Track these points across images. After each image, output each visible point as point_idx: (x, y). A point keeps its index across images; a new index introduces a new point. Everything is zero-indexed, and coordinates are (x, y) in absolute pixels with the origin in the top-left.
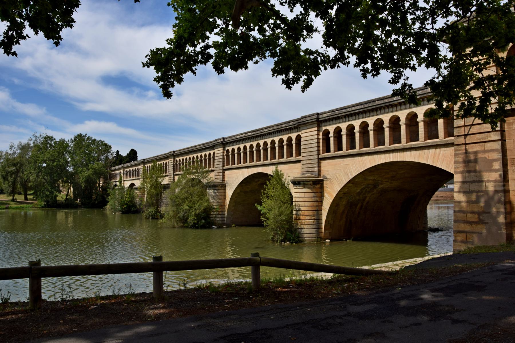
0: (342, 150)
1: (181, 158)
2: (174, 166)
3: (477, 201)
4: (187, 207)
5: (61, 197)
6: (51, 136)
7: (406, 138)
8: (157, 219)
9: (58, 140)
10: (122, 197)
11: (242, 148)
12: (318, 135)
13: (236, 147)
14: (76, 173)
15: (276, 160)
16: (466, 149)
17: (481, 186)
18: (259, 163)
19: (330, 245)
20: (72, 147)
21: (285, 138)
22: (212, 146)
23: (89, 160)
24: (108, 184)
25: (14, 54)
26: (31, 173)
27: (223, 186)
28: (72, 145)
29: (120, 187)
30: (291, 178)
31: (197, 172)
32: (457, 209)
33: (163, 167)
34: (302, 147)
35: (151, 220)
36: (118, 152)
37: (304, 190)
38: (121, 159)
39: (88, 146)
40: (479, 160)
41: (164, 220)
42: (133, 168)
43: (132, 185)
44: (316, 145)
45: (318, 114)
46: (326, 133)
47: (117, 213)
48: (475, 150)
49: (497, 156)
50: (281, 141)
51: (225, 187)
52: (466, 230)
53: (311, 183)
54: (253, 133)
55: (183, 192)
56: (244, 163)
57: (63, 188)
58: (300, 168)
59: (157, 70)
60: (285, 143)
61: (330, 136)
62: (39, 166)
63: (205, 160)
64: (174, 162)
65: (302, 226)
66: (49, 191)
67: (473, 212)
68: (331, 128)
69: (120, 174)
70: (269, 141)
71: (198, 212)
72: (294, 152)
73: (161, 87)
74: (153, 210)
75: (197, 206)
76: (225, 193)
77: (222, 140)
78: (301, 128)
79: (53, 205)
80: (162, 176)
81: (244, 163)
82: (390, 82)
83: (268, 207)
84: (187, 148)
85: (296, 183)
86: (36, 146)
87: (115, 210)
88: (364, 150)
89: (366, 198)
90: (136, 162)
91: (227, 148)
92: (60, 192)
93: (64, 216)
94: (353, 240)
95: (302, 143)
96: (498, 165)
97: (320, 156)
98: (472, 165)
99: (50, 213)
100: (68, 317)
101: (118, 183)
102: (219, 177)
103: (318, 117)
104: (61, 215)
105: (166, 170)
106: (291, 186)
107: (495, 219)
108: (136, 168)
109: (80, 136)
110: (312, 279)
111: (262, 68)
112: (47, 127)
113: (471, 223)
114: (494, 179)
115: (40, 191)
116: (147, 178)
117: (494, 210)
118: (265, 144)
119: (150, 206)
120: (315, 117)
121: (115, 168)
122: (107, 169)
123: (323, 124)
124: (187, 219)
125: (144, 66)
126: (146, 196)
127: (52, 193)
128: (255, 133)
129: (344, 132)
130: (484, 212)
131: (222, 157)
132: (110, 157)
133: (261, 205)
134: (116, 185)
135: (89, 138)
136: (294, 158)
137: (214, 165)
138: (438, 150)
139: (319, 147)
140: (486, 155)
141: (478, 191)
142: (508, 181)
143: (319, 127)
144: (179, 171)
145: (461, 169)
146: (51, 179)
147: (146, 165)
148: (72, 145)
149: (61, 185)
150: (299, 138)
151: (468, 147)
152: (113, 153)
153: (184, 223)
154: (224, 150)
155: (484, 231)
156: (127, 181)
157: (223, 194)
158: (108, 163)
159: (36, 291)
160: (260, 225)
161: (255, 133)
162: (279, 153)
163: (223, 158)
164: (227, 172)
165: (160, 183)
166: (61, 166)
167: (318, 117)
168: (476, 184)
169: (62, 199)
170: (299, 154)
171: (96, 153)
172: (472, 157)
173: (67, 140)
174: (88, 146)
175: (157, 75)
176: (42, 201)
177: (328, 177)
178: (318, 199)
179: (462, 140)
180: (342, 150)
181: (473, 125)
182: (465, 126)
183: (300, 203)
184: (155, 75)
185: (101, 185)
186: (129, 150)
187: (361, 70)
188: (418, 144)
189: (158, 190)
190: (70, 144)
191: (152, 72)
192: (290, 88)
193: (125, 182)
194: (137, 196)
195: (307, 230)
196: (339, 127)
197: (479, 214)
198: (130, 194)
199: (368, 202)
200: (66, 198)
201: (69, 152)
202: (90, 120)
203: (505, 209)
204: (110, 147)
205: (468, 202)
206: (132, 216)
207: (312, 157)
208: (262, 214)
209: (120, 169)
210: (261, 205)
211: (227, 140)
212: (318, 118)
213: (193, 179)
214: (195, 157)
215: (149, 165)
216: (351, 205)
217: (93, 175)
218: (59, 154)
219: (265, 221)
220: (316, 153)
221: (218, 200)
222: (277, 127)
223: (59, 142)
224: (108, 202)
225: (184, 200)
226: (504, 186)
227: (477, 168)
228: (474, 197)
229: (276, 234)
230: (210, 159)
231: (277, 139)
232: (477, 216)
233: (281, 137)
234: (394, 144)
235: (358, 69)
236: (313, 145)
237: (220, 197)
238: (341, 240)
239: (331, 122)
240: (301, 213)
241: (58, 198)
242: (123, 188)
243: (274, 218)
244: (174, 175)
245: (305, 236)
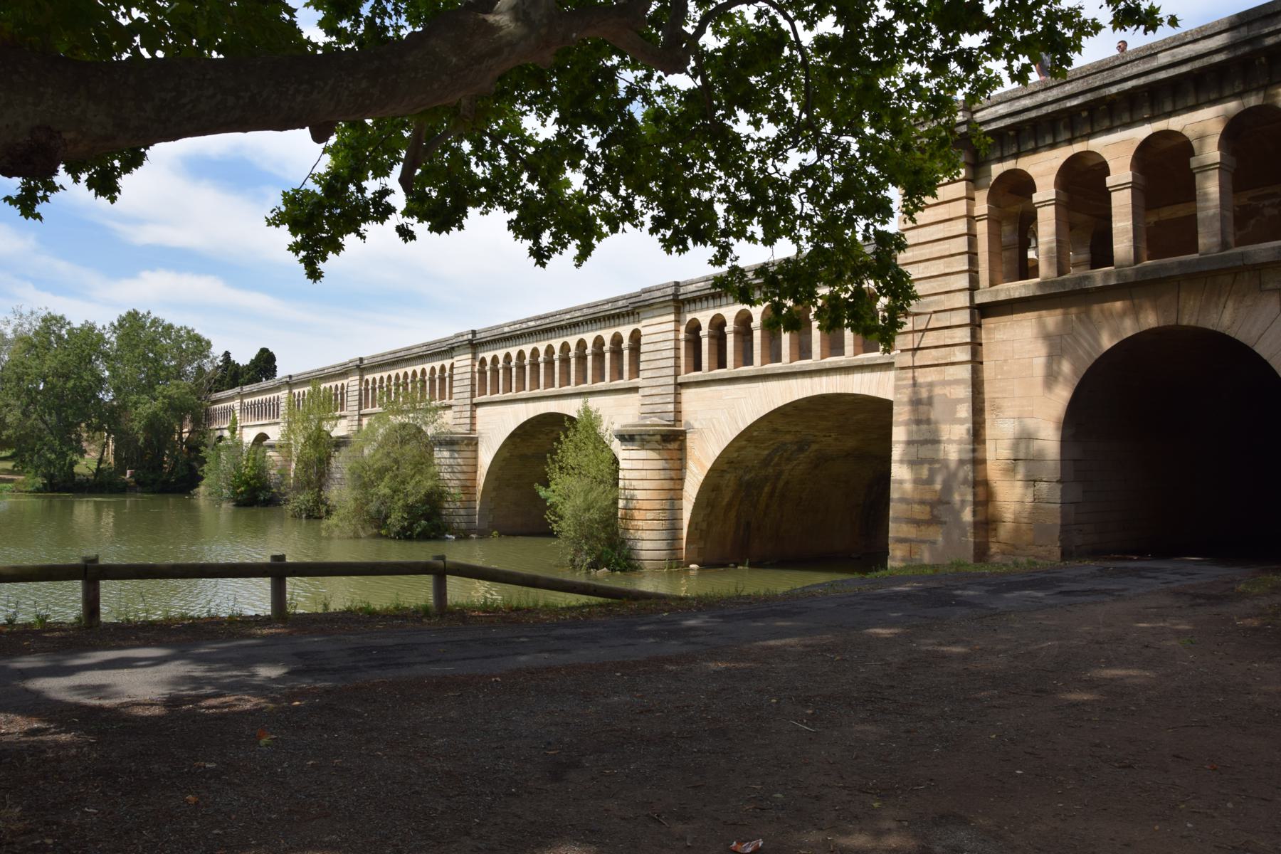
1: (377, 376)
2: (360, 394)
3: (930, 481)
4: (387, 491)
5: (86, 465)
6: (59, 314)
7: (855, 345)
8: (321, 518)
9: (77, 324)
10: (237, 467)
11: (514, 355)
12: (677, 331)
13: (501, 354)
14: (123, 407)
15: (588, 386)
16: (914, 378)
17: (937, 450)
18: (551, 391)
19: (699, 574)
20: (112, 344)
21: (607, 334)
22: (449, 350)
23: (156, 375)
24: (203, 434)
25: (38, 216)
26: (7, 405)
27: (471, 443)
28: (113, 339)
29: (230, 443)
30: (617, 427)
31: (415, 410)
33: (336, 395)
34: (643, 357)
35: (304, 521)
36: (227, 354)
38: (236, 373)
39: (154, 341)
40: (936, 400)
41: (333, 520)
42: (264, 397)
43: (262, 438)
44: (672, 353)
45: (677, 284)
46: (694, 328)
47: (224, 505)
48: (929, 379)
49: (964, 392)
50: (599, 342)
51: (477, 444)
52: (910, 536)
53: (658, 437)
54: (539, 323)
55: (378, 456)
56: (504, 392)
57: (90, 444)
58: (638, 404)
59: (294, 232)
60: (607, 347)
61: (726, 329)
62: (29, 390)
63: (432, 381)
64: (360, 384)
65: (639, 534)
66: (54, 451)
67: (922, 502)
69: (232, 410)
70: (572, 341)
71: (411, 500)
72: (626, 368)
73: (301, 261)
74: (309, 497)
75: (409, 488)
76: (476, 458)
77: (470, 336)
78: (642, 315)
79: (63, 485)
80: (332, 418)
81: (504, 392)
82: (710, 262)
83: (566, 493)
85: (627, 438)
86: (21, 339)
87: (217, 498)
88: (745, 370)
89: (780, 473)
90: (270, 383)
91: (481, 355)
92: (82, 453)
93: (92, 516)
94: (751, 565)
95: (643, 349)
96: (964, 411)
97: (680, 380)
98: (923, 408)
99: (57, 503)
100: (141, 635)
101: (227, 434)
102: (462, 421)
103: (677, 290)
104: (84, 510)
105: (342, 404)
106: (616, 446)
107: (957, 514)
108: (272, 396)
109: (133, 316)
111: (488, 228)
112: (45, 283)
114: (956, 438)
115: (33, 450)
116: (295, 422)
117: (957, 498)
118: (565, 347)
119: (303, 488)
120: (670, 291)
121: (219, 395)
122: (199, 398)
123: (687, 308)
124: (387, 517)
125: (269, 224)
126: (293, 465)
127: (62, 455)
128: (543, 321)
129: (730, 327)
131: (469, 375)
132: (208, 368)
133: (547, 485)
134: (221, 438)
135: (155, 322)
136: (625, 382)
137: (451, 393)
139: (677, 358)
140: (947, 391)
141: (932, 461)
142: (984, 442)
143: (678, 312)
144: (373, 406)
146: (60, 420)
147: (296, 391)
148: (113, 339)
149: (85, 435)
150: (636, 336)
152: (215, 358)
153: (379, 527)
154: (474, 358)
155: (940, 539)
156: (248, 426)
157: (471, 462)
158: (202, 384)
159: (92, 604)
160: (547, 532)
161: (543, 321)
162: (594, 369)
163: (473, 378)
164: (480, 411)
165: (328, 434)
166: (84, 390)
167: (677, 290)
168: (929, 446)
169: (86, 471)
170: (635, 372)
171: (173, 358)
172: (924, 394)
173: (99, 326)
174: (154, 341)
175: (294, 239)
176: (36, 475)
177: (696, 425)
178: (673, 474)
179: (907, 360)
183: (634, 483)
184: (291, 239)
185: (185, 436)
186: (256, 351)
187: (661, 240)
188: (876, 358)
189: (322, 450)
190: (107, 336)
191: (284, 235)
192: (543, 265)
194: (274, 465)
195: (648, 541)
196: (719, 315)
197: (933, 505)
198: (254, 459)
199: (787, 483)
200: (98, 469)
201: (106, 356)
202: (153, 270)
203: (975, 495)
204: (209, 344)
205: (917, 481)
206: (261, 512)
207: (661, 381)
208: (549, 508)
209: (232, 398)
210: (547, 485)
211: (483, 335)
212: (676, 295)
213: (404, 426)
214: (410, 374)
215: (301, 390)
216: (748, 489)
217: (166, 411)
218: (81, 359)
219: (555, 522)
221: (459, 476)
222: (591, 311)
223: (81, 330)
224: (202, 478)
225: (381, 473)
226: (974, 450)
227: (933, 417)
228: (925, 472)
229: (578, 551)
230: (442, 379)
231: (589, 338)
232: (928, 508)
233: (598, 333)
234: (831, 355)
235: (656, 237)
236: (665, 354)
237: (465, 468)
238: (725, 566)
239: (705, 304)
241: (76, 469)
242: (239, 444)
243: (574, 516)
244: (361, 416)
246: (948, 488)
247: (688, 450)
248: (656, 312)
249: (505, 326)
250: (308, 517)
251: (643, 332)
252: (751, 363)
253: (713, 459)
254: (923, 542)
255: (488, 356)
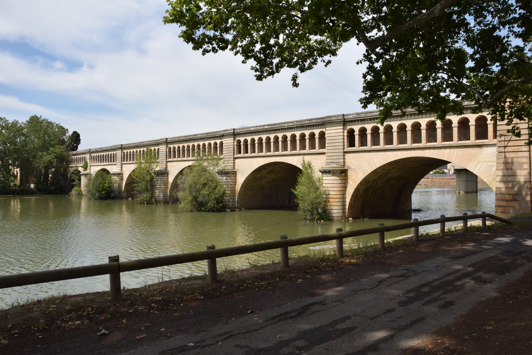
0: (354, 146)
1: (95, 155)
3: (513, 187)
11: (138, 151)
17: (516, 178)
27: (235, 173)
32: (498, 192)
37: (334, 178)
40: (515, 163)
46: (239, 142)
48: (512, 156)
51: (236, 173)
65: (332, 207)
67: (509, 194)
68: (357, 128)
69: (84, 159)
76: (236, 179)
84: (184, 137)
85: (324, 172)
88: (294, 152)
91: (169, 146)
94: (369, 218)
95: (224, 147)
107: (524, 199)
110: (395, 241)
113: (507, 201)
117: (524, 193)
120: (232, 131)
130: (516, 194)
138: (452, 150)
140: (519, 160)
141: (513, 182)
143: (344, 125)
145: (502, 168)
151: (506, 154)
155: (517, 206)
157: (234, 180)
170: (221, 153)
172: (510, 160)
173: (20, 122)
177: (352, 167)
180: (354, 146)
181: (510, 140)
182: (505, 141)
193: (92, 167)
194: (115, 183)
195: (336, 211)
197: (513, 195)
205: (507, 188)
206: (110, 201)
211: (238, 131)
212: (234, 133)
214: (138, 151)
220: (342, 147)
221: (229, 186)
232: (512, 196)
233: (260, 136)
238: (359, 218)
240: (331, 196)
245: (334, 215)
246: (520, 190)
247: (349, 176)
248: (333, 125)
249: (251, 127)
250: (148, 203)
251: (224, 142)
252: (315, 149)
253: (361, 180)
254: (510, 207)
255: (242, 139)
